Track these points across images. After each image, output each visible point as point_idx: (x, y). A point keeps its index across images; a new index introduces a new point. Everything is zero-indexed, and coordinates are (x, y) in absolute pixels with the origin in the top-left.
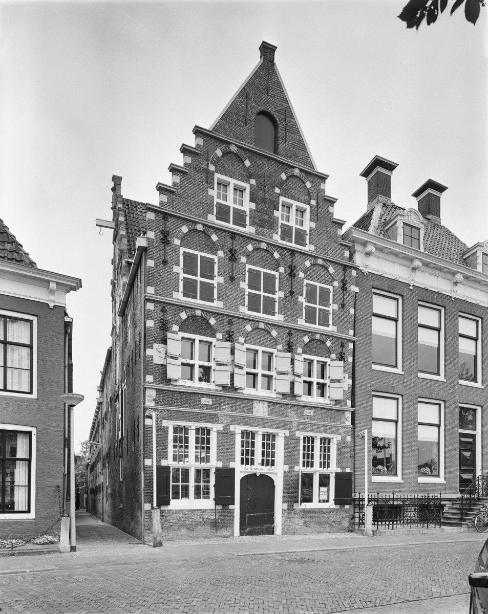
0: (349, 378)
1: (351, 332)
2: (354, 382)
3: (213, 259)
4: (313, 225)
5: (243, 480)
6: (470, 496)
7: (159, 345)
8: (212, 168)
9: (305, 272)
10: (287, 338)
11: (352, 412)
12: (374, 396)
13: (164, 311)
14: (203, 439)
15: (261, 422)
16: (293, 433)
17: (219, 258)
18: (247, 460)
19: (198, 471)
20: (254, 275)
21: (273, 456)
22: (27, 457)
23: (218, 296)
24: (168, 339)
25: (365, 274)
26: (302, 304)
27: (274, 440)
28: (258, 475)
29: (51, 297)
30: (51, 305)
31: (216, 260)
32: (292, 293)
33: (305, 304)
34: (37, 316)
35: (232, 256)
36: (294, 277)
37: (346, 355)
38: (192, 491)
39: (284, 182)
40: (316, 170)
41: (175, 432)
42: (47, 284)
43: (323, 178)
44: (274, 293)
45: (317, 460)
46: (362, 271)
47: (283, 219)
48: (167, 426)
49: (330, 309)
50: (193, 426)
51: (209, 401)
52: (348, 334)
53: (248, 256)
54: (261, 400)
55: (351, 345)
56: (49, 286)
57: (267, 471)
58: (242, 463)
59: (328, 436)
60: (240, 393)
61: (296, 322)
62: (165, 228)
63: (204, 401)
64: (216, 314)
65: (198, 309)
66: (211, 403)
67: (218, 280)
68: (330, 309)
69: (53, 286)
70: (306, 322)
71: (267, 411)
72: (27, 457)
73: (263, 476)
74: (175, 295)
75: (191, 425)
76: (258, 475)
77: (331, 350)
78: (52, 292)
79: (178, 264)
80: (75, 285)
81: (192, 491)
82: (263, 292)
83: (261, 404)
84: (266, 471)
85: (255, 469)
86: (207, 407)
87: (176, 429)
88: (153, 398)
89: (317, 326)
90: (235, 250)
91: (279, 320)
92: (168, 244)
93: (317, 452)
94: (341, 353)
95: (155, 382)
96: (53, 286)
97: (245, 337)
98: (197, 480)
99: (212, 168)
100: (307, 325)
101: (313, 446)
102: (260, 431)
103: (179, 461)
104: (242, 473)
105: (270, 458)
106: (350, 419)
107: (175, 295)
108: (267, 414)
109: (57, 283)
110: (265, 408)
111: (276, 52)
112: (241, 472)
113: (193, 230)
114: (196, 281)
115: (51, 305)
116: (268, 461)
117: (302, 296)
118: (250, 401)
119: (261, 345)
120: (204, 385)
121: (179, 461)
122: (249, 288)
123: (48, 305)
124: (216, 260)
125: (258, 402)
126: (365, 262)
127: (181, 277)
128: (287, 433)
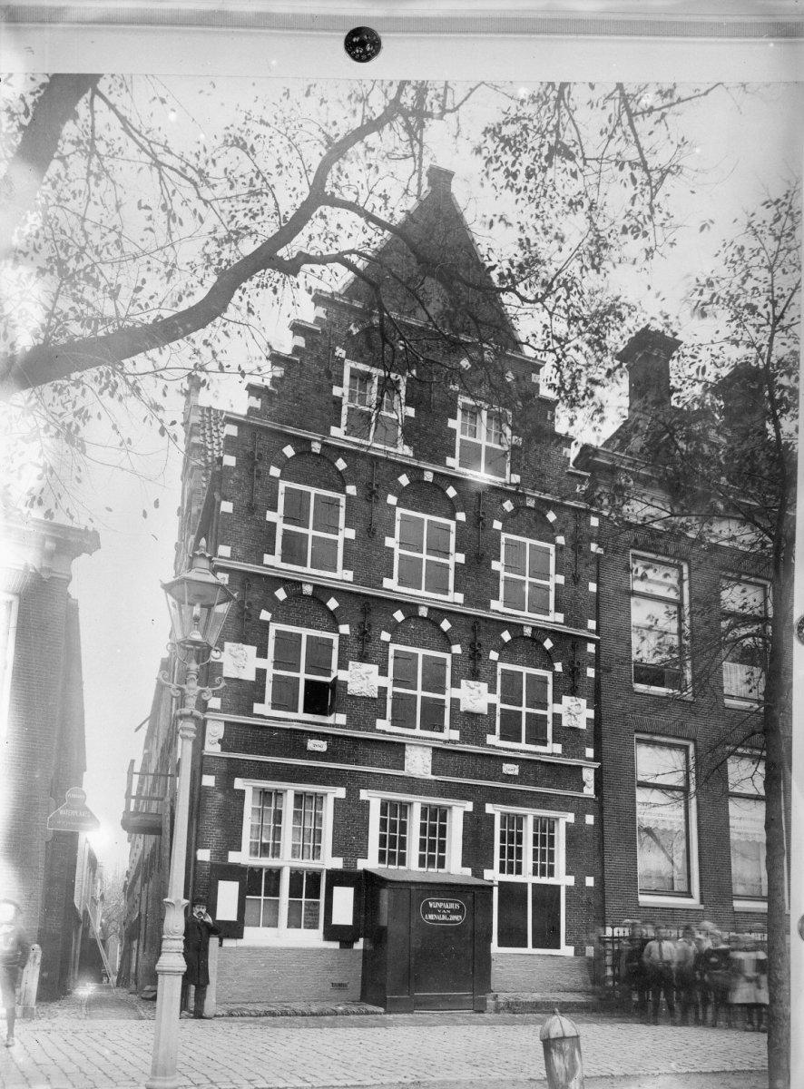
0: (588, 707)
2: (598, 713)
3: (449, 526)
9: (503, 520)
10: (468, 635)
11: (595, 769)
12: (640, 741)
14: (511, 835)
15: (413, 785)
19: (296, 876)
21: (442, 849)
22: (686, 890)
23: (556, 607)
26: (273, 525)
27: (444, 818)
35: (371, 494)
44: (446, 554)
45: (528, 861)
47: (463, 433)
49: (551, 584)
50: (530, 814)
51: (321, 746)
53: (505, 518)
55: (591, 648)
59: (277, 787)
61: (378, 584)
63: (313, 745)
64: (554, 634)
65: (307, 583)
66: (324, 748)
72: (686, 890)
74: (387, 583)
75: (327, 791)
77: (451, 636)
82: (307, 535)
86: (509, 778)
93: (528, 846)
95: (224, 709)
99: (341, 352)
101: (553, 837)
102: (417, 802)
105: (436, 854)
106: (593, 782)
108: (429, 770)
111: (453, 182)
114: (306, 536)
116: (511, 864)
119: (423, 645)
127: (502, 577)
128: (469, 806)
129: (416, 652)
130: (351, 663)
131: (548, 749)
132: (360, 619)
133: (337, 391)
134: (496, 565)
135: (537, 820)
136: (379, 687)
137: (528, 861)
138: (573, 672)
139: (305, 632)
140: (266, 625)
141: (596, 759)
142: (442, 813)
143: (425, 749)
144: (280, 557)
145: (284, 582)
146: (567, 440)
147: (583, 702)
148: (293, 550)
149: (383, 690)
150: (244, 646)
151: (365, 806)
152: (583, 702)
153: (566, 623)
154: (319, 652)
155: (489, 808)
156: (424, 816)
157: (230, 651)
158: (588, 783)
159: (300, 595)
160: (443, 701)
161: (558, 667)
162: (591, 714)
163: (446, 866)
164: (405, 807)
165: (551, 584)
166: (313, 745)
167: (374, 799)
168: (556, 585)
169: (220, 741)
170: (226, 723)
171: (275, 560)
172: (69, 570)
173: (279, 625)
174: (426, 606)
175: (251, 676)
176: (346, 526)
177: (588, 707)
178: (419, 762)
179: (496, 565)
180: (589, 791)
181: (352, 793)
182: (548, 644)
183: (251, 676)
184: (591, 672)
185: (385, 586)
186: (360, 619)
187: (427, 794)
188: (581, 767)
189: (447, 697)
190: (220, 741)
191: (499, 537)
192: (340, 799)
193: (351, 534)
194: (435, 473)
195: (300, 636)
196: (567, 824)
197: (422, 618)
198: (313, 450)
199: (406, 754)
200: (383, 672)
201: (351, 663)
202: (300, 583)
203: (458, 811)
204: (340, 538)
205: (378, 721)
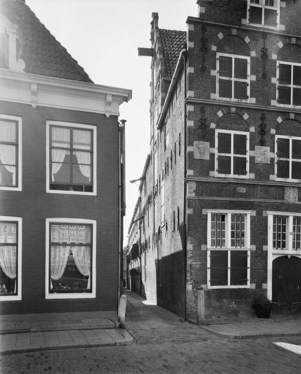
5: (275, 262)
6: (249, 268)
13: (203, 111)
17: (252, 58)
18: (280, 243)
20: (225, 63)
28: (289, 257)
29: (108, 108)
30: (108, 115)
31: (249, 61)
32: (265, 76)
33: (218, 77)
34: (21, 116)
37: (268, 127)
42: (103, 96)
49: (248, 81)
51: (243, 190)
56: (106, 99)
58: (274, 246)
62: (203, 36)
64: (249, 110)
67: (250, 78)
68: (248, 81)
69: (109, 98)
71: (297, 197)
75: (246, 213)
76: (289, 257)
78: (109, 104)
79: (215, 68)
80: (127, 96)
83: (292, 190)
86: (242, 195)
88: (193, 190)
90: (206, 39)
94: (262, 125)
96: (109, 98)
97: (275, 129)
100: (282, 105)
104: (275, 255)
107: (213, 96)
108: (297, 199)
109: (113, 96)
110: (295, 194)
112: (273, 254)
115: (108, 115)
118: (282, 188)
122: (220, 75)
123: (105, 115)
124: (249, 61)
125: (289, 188)
129: (230, 133)
130: (256, 147)
131: (247, 177)
132: (260, 122)
134: (214, 73)
135: (233, 216)
136: (270, 158)
138: (263, 131)
139: (233, 133)
140: (213, 131)
142: (284, 219)
144: (218, 95)
145: (220, 107)
148: (225, 90)
149: (272, 160)
154: (241, 141)
156: (233, 219)
157: (197, 145)
160: (245, 158)
161: (252, 129)
163: (286, 247)
164: (223, 217)
166: (243, 190)
167: (270, 216)
168: (251, 81)
169: (194, 191)
171: (216, 96)
172: (118, 111)
173: (220, 130)
175: (207, 157)
178: (291, 196)
179: (214, 73)
181: (259, 213)
182: (246, 117)
183: (207, 157)
185: (211, 98)
186: (260, 122)
187: (296, 211)
189: (247, 157)
191: (276, 63)
192: (253, 216)
193: (254, 78)
195: (230, 135)
196: (251, 217)
197: (292, 119)
198: (233, 34)
200: (272, 150)
201: (256, 147)
203: (249, 214)
205: (271, 175)
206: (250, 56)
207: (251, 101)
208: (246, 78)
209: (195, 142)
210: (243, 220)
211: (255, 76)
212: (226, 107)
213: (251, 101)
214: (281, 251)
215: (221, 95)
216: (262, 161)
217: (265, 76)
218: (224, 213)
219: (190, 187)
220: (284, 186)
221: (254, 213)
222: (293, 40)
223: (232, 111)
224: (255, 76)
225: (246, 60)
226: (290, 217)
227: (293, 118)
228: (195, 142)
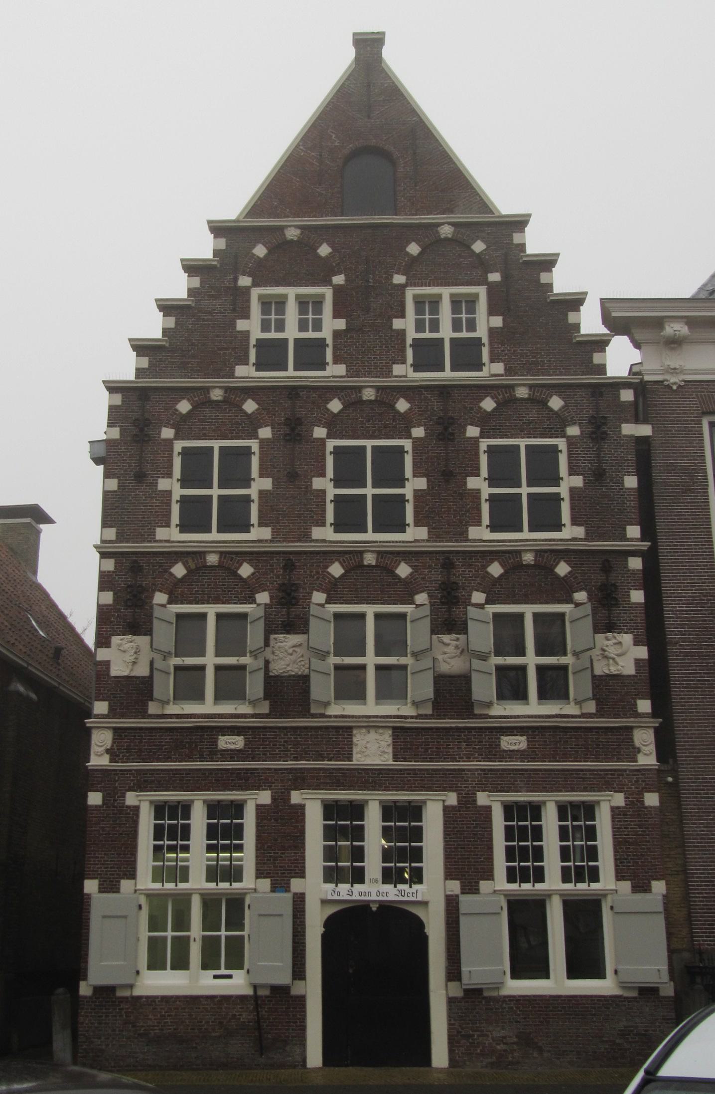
0: (636, 643)
1: (634, 531)
3: (250, 448)
4: (497, 322)
7: (122, 637)
8: (245, 281)
16: (467, 801)
23: (260, 517)
24: (469, 622)
25: (675, 387)
28: (374, 908)
36: (453, 440)
38: (195, 952)
39: (414, 260)
40: (497, 214)
41: (508, 817)
43: (520, 223)
45: (552, 863)
46: (666, 383)
48: (136, 803)
51: (237, 742)
52: (624, 537)
54: (372, 724)
57: (396, 898)
60: (481, 716)
63: (226, 742)
70: (336, 531)
73: (388, 910)
76: (374, 908)
81: (195, 952)
83: (373, 735)
84: (392, 897)
85: (360, 894)
86: (512, 755)
87: (509, 810)
89: (526, 534)
91: (416, 541)
92: (603, 439)
95: (113, 712)
98: (210, 923)
99: (245, 281)
103: (576, 882)
107: (474, 532)
108: (390, 756)
112: (324, 902)
113: (203, 404)
117: (478, 475)
119: (526, 600)
120: (551, 708)
121: (576, 882)
126: (667, 363)
133: (397, 324)
137: (552, 863)
141: (655, 714)
143: (381, 731)
146: (575, 302)
147: (627, 639)
150: (135, 637)
151: (299, 812)
152: (627, 639)
153: (589, 537)
155: (482, 799)
158: (645, 749)
159: (520, 567)
162: (642, 652)
164: (536, 811)
165: (408, 492)
166: (226, 742)
169: (108, 751)
170: (115, 730)
174: (372, 551)
176: (261, 476)
177: (636, 643)
180: (648, 758)
184: (637, 596)
188: (630, 729)
190: (108, 751)
194: (378, 389)
196: (613, 809)
199: (355, 740)
202: (361, 553)
204: (563, 490)
206: (569, 437)
207: (259, 533)
208: (249, 487)
209: (115, 640)
210: (187, 815)
211: (424, 480)
212: (511, 558)
213: (259, 533)
214: (345, 891)
215: (184, 527)
216: (289, 668)
217: (140, 477)
218: (592, 801)
219: (643, 743)
220: (351, 728)
221: (619, 799)
222: (366, 393)
223: (210, 562)
224: (424, 480)
225: (250, 448)
226: (370, 802)
227: (374, 564)
228: (115, 640)
